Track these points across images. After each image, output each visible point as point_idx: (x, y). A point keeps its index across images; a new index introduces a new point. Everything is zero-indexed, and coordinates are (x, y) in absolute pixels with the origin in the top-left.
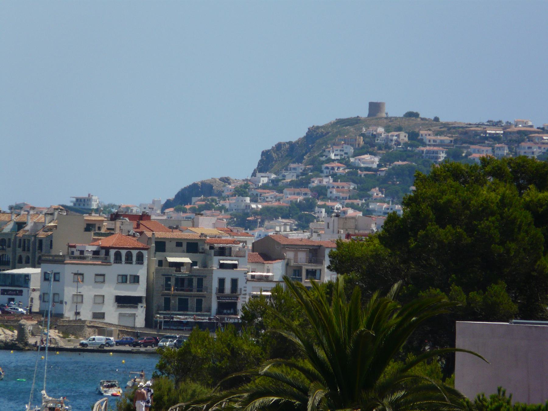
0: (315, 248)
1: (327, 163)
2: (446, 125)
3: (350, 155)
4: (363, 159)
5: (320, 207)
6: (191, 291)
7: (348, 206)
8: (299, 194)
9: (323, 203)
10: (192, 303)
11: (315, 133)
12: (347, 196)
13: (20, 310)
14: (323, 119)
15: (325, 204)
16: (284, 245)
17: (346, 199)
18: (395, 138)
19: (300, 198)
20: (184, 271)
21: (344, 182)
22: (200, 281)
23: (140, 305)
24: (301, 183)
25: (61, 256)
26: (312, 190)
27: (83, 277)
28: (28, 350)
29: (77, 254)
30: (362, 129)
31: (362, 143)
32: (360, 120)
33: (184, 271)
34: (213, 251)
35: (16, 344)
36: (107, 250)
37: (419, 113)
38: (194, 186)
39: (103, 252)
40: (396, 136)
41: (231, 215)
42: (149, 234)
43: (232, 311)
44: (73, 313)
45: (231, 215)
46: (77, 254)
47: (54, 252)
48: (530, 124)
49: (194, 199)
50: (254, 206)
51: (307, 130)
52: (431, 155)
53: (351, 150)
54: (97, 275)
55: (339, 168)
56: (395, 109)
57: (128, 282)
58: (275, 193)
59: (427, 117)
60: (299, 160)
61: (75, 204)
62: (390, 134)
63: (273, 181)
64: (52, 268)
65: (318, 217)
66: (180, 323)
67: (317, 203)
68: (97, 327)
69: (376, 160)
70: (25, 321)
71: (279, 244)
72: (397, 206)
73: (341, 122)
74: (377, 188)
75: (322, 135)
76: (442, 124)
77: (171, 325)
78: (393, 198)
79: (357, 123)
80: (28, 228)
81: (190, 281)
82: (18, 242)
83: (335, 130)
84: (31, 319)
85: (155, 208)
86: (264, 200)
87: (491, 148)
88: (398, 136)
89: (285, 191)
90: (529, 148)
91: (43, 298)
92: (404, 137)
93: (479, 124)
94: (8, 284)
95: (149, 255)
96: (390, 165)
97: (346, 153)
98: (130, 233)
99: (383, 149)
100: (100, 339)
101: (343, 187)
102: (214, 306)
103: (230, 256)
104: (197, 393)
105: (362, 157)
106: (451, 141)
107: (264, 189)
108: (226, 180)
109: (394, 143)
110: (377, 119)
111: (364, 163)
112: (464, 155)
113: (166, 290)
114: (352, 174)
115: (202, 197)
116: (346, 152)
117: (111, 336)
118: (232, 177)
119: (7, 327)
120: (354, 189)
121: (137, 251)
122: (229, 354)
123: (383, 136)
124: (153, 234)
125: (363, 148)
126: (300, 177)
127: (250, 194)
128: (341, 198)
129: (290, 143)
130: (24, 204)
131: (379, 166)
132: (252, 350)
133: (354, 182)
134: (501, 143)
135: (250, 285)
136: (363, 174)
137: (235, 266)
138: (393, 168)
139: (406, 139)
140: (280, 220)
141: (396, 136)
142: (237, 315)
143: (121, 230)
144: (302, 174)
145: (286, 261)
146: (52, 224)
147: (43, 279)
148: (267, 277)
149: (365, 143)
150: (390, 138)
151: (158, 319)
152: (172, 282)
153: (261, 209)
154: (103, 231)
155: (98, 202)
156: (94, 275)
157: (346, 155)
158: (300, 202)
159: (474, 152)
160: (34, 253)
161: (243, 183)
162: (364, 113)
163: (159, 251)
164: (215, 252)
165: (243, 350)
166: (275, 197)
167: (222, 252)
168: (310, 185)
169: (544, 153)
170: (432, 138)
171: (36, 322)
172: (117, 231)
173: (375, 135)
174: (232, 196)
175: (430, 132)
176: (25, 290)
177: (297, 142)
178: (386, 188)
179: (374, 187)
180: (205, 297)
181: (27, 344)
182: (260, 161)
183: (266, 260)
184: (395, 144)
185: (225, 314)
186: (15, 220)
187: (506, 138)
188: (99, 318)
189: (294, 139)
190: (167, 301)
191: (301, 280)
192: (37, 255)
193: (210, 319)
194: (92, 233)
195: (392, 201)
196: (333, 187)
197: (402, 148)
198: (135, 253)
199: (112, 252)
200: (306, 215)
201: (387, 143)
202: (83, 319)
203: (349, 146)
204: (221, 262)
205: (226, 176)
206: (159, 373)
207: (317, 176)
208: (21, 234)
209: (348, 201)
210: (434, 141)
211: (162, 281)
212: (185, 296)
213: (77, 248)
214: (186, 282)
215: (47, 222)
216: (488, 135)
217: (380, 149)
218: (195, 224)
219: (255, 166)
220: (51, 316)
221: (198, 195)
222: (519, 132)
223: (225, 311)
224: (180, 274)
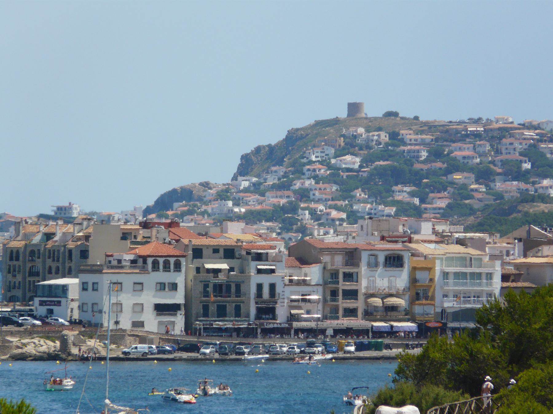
0: (351, 250)
1: (308, 165)
2: (425, 124)
3: (331, 156)
4: (344, 160)
5: (304, 209)
6: (230, 297)
7: (330, 207)
8: (281, 197)
9: (306, 205)
10: (230, 309)
11: (295, 135)
12: (330, 197)
13: (61, 320)
14: (303, 120)
15: (308, 207)
16: (321, 249)
17: (329, 200)
18: (376, 138)
19: (283, 201)
20: (222, 277)
21: (326, 183)
22: (238, 286)
23: (179, 312)
24: (283, 186)
25: (99, 265)
26: (295, 192)
27: (143, 286)
28: (72, 360)
29: (115, 263)
30: (342, 129)
31: (342, 144)
32: (339, 121)
33: (222, 277)
34: (250, 257)
35: (60, 355)
36: (145, 258)
37: (398, 111)
38: (174, 191)
39: (141, 260)
40: (377, 136)
41: (214, 219)
42: (186, 241)
43: (271, 316)
44: (112, 322)
45: (214, 219)
46: (115, 263)
47: (90, 261)
48: (510, 120)
49: (176, 205)
50: (236, 210)
51: (286, 133)
52: (412, 154)
53: (332, 151)
54: (135, 283)
55: (320, 170)
56: (373, 110)
57: (167, 289)
58: (257, 196)
59: (408, 116)
60: (280, 162)
61: (56, 213)
62: (371, 134)
63: (254, 184)
64: (90, 278)
65: (302, 219)
66: (220, 330)
67: (300, 205)
68: (137, 336)
69: (358, 160)
70: (67, 331)
71: (315, 248)
72: (380, 207)
73: (320, 124)
74: (360, 189)
75: (302, 137)
76: (422, 123)
77: (210, 331)
78: (376, 198)
79: (336, 124)
80: (57, 238)
81: (229, 287)
82: (47, 254)
83: (315, 132)
84: (72, 330)
85: (136, 214)
86: (247, 204)
87: (472, 145)
88: (379, 136)
89: (267, 194)
90: (511, 144)
91: (81, 308)
92: (384, 137)
93: (459, 122)
94: (46, 295)
95: (186, 262)
96: (371, 165)
97: (326, 155)
98: (166, 241)
99: (364, 149)
100: (143, 347)
101: (325, 189)
102: (253, 312)
103: (267, 260)
104: (440, 397)
105: (344, 158)
106: (432, 140)
107: (245, 192)
108: (206, 185)
109: (374, 142)
110: (356, 119)
111: (345, 164)
112: (445, 153)
113: (205, 296)
114: (335, 175)
115: (184, 202)
116: (327, 153)
117: (152, 344)
118: (212, 181)
119: (48, 338)
120: (337, 190)
121: (164, 259)
122: (468, 358)
123: (364, 136)
124: (190, 241)
125: (344, 149)
126: (282, 180)
127: (231, 197)
128: (324, 199)
129: (269, 146)
130: (5, 214)
131: (361, 166)
132: (491, 353)
133: (335, 183)
134: (482, 140)
135: (288, 289)
136: (345, 175)
137: (272, 271)
138: (375, 169)
139: (387, 139)
140: (263, 223)
141: (377, 136)
142: (276, 320)
143: (157, 238)
144: (284, 177)
145: (323, 264)
146: (81, 234)
147: (81, 289)
148: (304, 281)
149: (345, 144)
150: (371, 138)
151: (197, 326)
152: (210, 289)
153: (244, 213)
154: (139, 239)
155: (78, 211)
156: (132, 284)
157: (327, 157)
158: (283, 205)
159: (456, 150)
160: (24, 262)
161: (224, 187)
162: (343, 114)
163: (197, 258)
164: (252, 257)
165: (481, 353)
166: (258, 200)
167: (259, 257)
168: (292, 188)
169: (525, 149)
170: (413, 137)
171: (77, 332)
172: (154, 239)
173: (355, 136)
174: (214, 200)
175: (411, 132)
176: (63, 300)
177: (277, 145)
178: (369, 189)
179: (357, 188)
180: (244, 302)
181: (69, 354)
182: (240, 165)
183: (302, 264)
184: (376, 144)
185: (264, 319)
186: (43, 231)
187: (487, 135)
188: (139, 326)
189: (273, 143)
190: (206, 308)
191: (338, 283)
192: (67, 265)
193: (249, 324)
194: (129, 242)
195: (376, 202)
196: (316, 189)
197: (383, 147)
198: (172, 260)
199: (150, 261)
200: (289, 218)
201: (368, 143)
202: (124, 328)
203: (330, 148)
204: (259, 267)
205: (206, 181)
206: (397, 377)
207: (299, 178)
208: (50, 244)
209: (330, 203)
210: (416, 140)
211: (200, 288)
212: (223, 302)
213: (115, 257)
214: (224, 288)
215: (76, 232)
216: (469, 132)
217: (361, 149)
218: (223, 231)
219: (235, 170)
220: (89, 326)
221: (178, 201)
222: (500, 129)
223: (264, 316)
224: (219, 280)
